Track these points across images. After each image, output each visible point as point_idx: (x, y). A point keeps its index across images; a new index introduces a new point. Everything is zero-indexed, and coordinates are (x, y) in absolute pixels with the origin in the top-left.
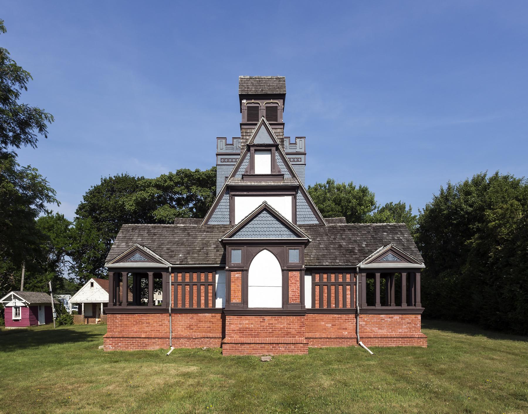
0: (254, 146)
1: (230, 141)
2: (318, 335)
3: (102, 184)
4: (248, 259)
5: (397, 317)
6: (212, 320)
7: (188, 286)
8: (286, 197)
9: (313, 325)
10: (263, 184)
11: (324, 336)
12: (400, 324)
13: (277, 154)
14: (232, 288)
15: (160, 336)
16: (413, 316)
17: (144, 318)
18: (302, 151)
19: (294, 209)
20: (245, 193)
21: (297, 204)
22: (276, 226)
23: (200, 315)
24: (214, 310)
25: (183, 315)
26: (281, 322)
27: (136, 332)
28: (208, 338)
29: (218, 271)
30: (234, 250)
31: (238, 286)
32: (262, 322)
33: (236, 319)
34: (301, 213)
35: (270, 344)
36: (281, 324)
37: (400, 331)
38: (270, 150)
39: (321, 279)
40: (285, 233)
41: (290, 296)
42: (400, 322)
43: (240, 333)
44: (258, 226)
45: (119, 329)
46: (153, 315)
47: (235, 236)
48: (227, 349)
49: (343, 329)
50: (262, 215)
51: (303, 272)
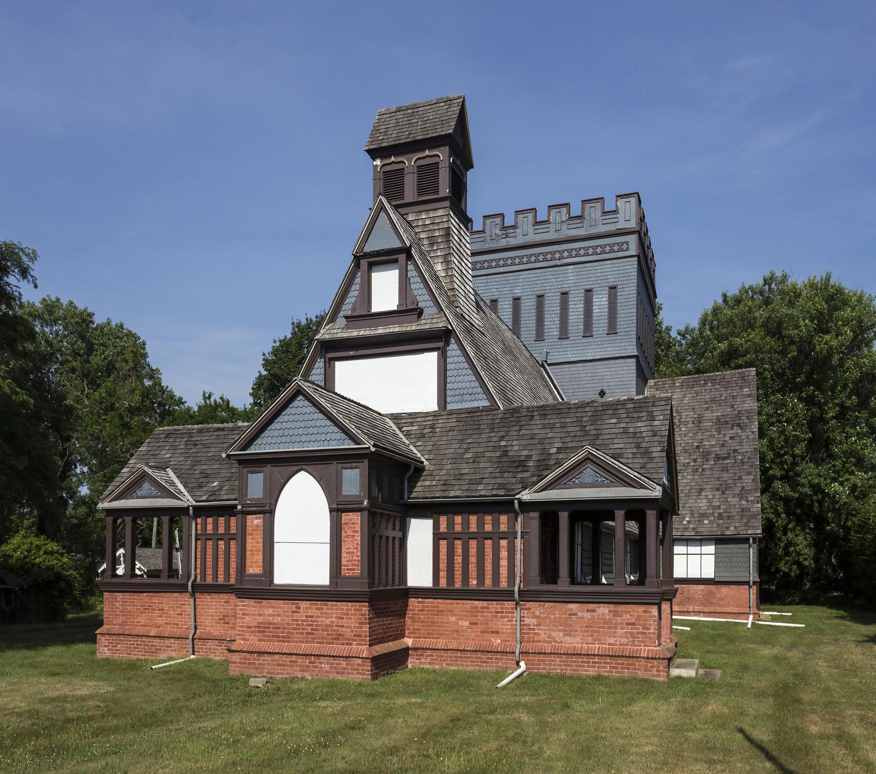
0: (367, 255)
1: (576, 211)
2: (441, 643)
3: (294, 334)
5: (603, 610)
8: (426, 354)
9: (433, 622)
10: (381, 331)
11: (453, 645)
12: (610, 626)
13: (411, 267)
14: (249, 547)
15: (178, 635)
16: (641, 609)
21: (449, 367)
22: (318, 423)
25: (214, 595)
26: (327, 613)
30: (252, 473)
31: (258, 542)
32: (295, 612)
33: (253, 606)
34: (455, 386)
35: (305, 655)
36: (326, 618)
37: (612, 640)
38: (396, 261)
39: (451, 524)
40: (334, 436)
41: (344, 562)
42: (610, 621)
43: (259, 632)
46: (168, 594)
47: (253, 447)
48: (236, 663)
49: (492, 632)
50: (296, 403)
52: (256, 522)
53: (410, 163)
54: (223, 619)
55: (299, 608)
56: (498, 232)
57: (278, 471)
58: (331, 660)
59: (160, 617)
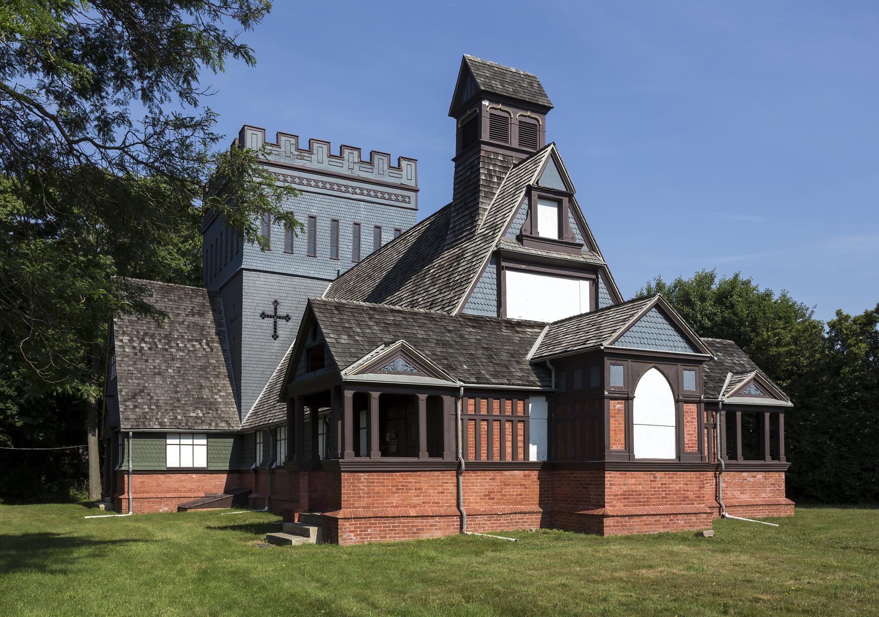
4: (632, 381)
5: (760, 476)
6: (524, 482)
7: (485, 423)
12: (763, 486)
17: (412, 479)
18: (412, 184)
19: (594, 303)
20: (523, 267)
22: (668, 332)
23: (505, 473)
24: (526, 465)
25: (479, 473)
27: (397, 507)
28: (521, 513)
29: (531, 398)
31: (620, 424)
37: (764, 495)
44: (645, 330)
45: (364, 502)
46: (428, 473)
50: (650, 313)
51: (702, 405)
52: (618, 406)
53: (515, 115)
54: (488, 495)
55: (656, 477)
56: (293, 151)
57: (637, 365)
58: (685, 517)
59: (418, 496)
